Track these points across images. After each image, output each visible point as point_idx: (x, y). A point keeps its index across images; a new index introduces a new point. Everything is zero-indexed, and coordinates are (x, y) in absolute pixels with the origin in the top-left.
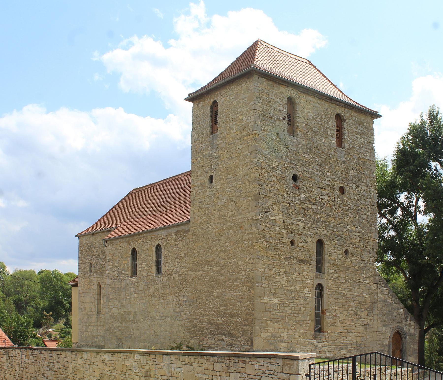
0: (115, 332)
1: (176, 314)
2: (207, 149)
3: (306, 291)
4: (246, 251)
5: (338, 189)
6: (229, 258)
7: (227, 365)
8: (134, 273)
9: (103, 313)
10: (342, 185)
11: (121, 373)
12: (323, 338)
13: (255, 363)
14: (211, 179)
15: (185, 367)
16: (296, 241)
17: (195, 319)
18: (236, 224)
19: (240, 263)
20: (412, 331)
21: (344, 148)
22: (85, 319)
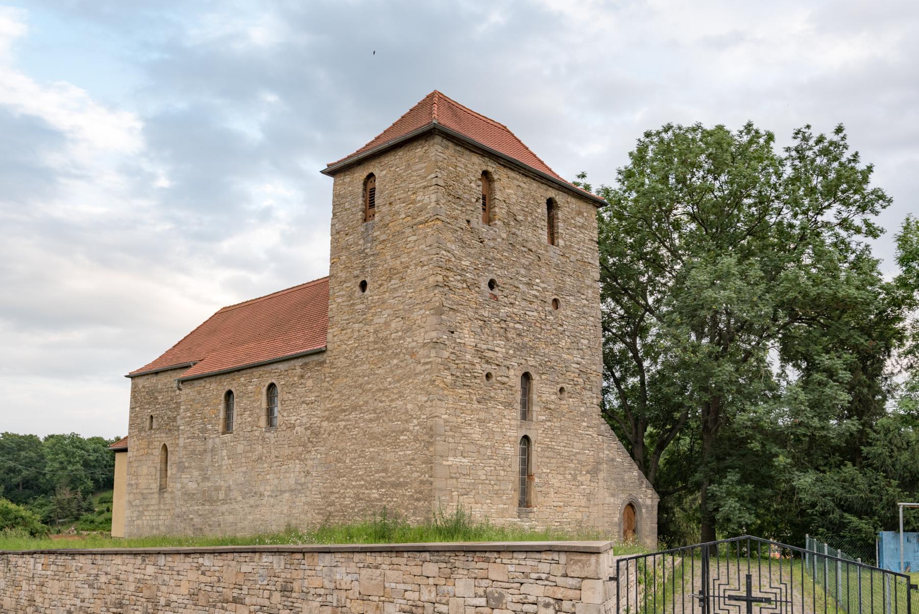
0: (192, 519)
1: (299, 487)
2: (357, 244)
3: (508, 447)
4: (421, 389)
5: (550, 302)
6: (392, 401)
7: (449, 565)
8: (228, 428)
9: (170, 490)
10: (556, 297)
11: (232, 586)
12: (531, 515)
13: (509, 561)
14: (363, 286)
15: (364, 572)
16: (494, 374)
17: (332, 493)
18: (404, 351)
19: (410, 406)
20: (649, 502)
21: (558, 246)
22: (137, 501)
